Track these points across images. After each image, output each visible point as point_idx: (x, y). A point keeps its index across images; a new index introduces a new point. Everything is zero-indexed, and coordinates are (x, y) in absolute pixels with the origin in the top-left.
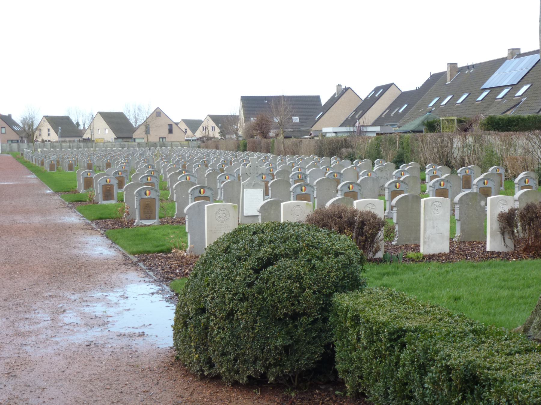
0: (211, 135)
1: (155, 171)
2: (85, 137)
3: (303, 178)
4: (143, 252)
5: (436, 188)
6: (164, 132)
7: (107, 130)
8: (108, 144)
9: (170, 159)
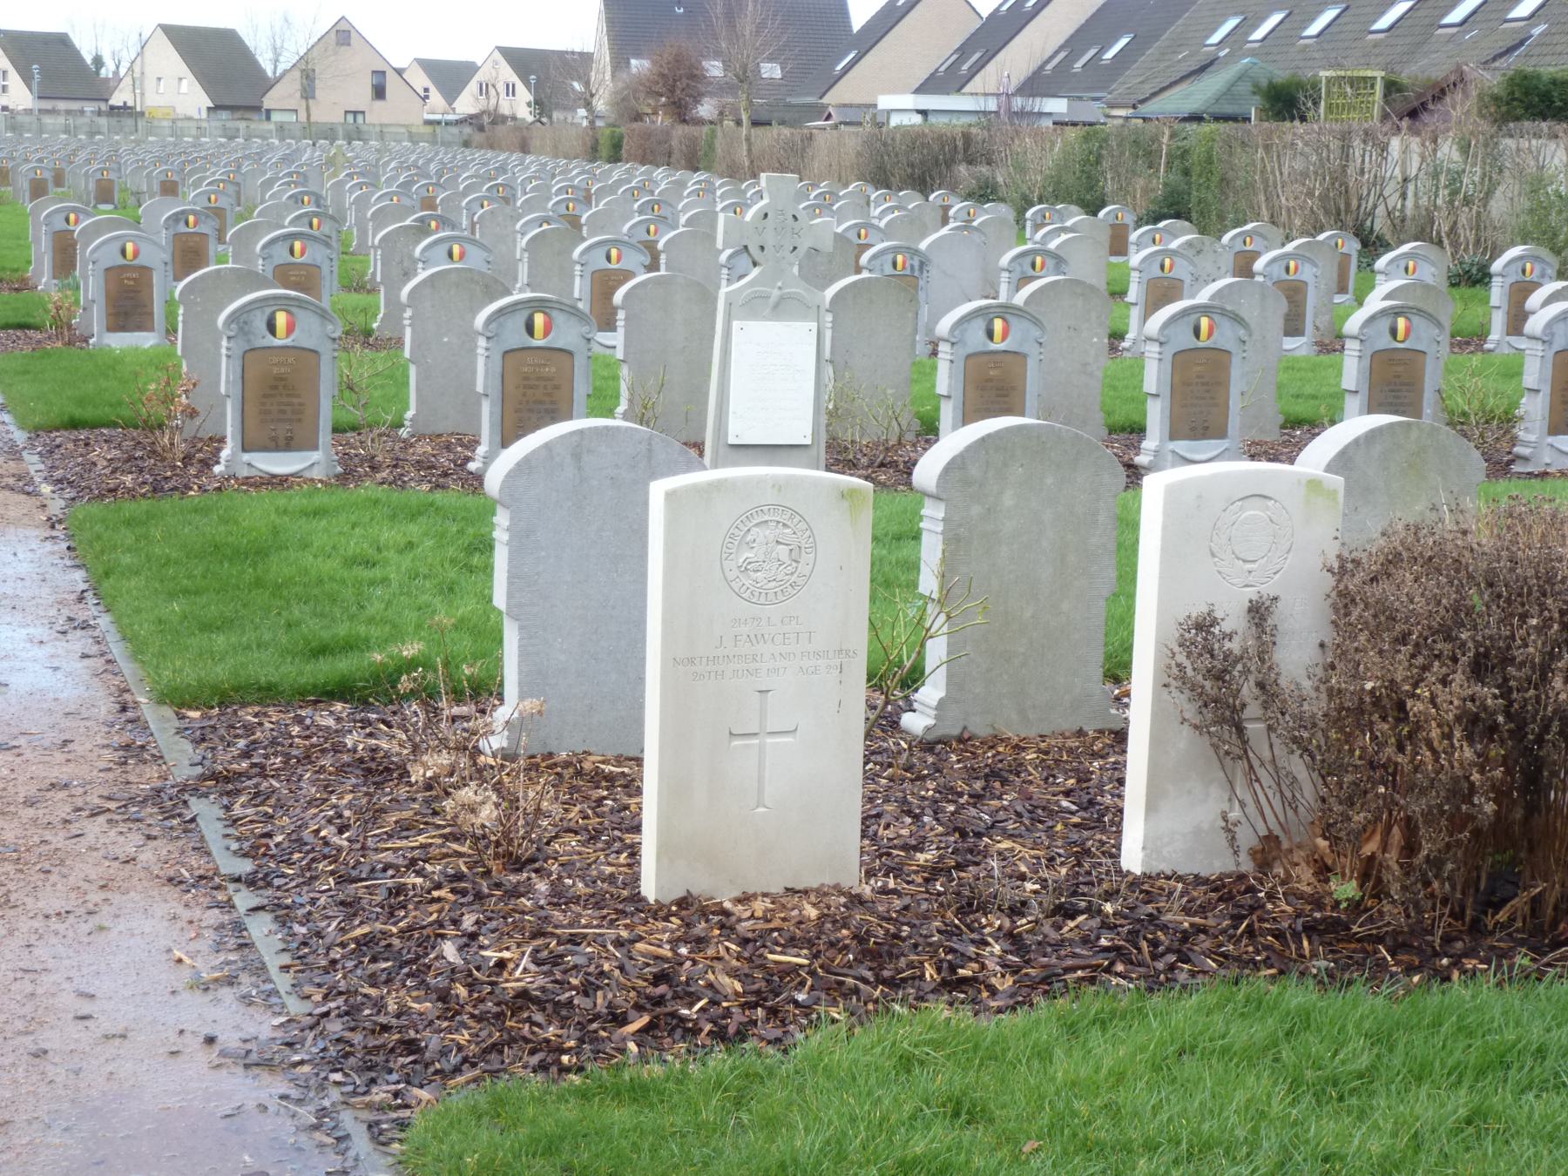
0: (505, 109)
1: (326, 215)
2: (117, 100)
3: (912, 267)
4: (237, 689)
5: (1557, 347)
6: (360, 95)
7: (185, 82)
8: (186, 124)
9: (377, 177)
